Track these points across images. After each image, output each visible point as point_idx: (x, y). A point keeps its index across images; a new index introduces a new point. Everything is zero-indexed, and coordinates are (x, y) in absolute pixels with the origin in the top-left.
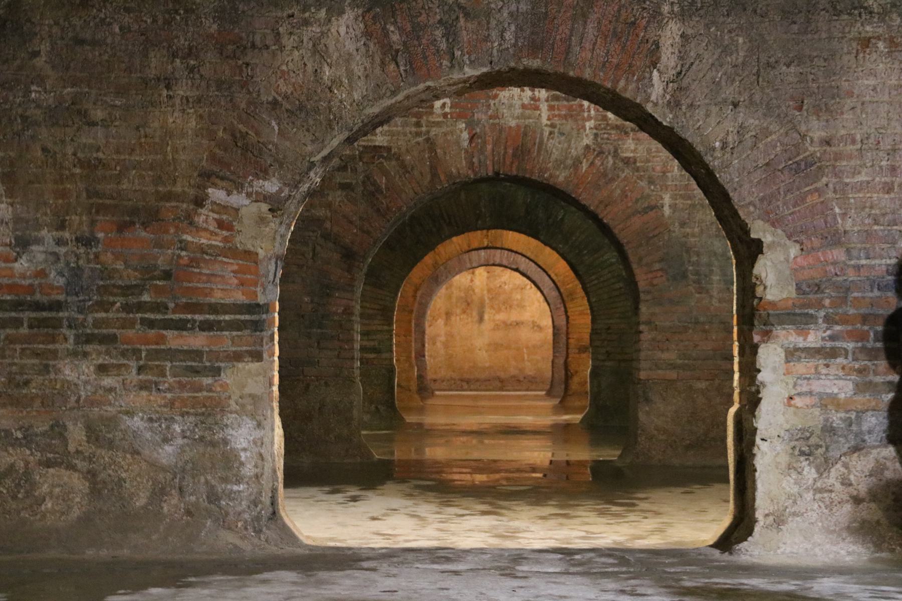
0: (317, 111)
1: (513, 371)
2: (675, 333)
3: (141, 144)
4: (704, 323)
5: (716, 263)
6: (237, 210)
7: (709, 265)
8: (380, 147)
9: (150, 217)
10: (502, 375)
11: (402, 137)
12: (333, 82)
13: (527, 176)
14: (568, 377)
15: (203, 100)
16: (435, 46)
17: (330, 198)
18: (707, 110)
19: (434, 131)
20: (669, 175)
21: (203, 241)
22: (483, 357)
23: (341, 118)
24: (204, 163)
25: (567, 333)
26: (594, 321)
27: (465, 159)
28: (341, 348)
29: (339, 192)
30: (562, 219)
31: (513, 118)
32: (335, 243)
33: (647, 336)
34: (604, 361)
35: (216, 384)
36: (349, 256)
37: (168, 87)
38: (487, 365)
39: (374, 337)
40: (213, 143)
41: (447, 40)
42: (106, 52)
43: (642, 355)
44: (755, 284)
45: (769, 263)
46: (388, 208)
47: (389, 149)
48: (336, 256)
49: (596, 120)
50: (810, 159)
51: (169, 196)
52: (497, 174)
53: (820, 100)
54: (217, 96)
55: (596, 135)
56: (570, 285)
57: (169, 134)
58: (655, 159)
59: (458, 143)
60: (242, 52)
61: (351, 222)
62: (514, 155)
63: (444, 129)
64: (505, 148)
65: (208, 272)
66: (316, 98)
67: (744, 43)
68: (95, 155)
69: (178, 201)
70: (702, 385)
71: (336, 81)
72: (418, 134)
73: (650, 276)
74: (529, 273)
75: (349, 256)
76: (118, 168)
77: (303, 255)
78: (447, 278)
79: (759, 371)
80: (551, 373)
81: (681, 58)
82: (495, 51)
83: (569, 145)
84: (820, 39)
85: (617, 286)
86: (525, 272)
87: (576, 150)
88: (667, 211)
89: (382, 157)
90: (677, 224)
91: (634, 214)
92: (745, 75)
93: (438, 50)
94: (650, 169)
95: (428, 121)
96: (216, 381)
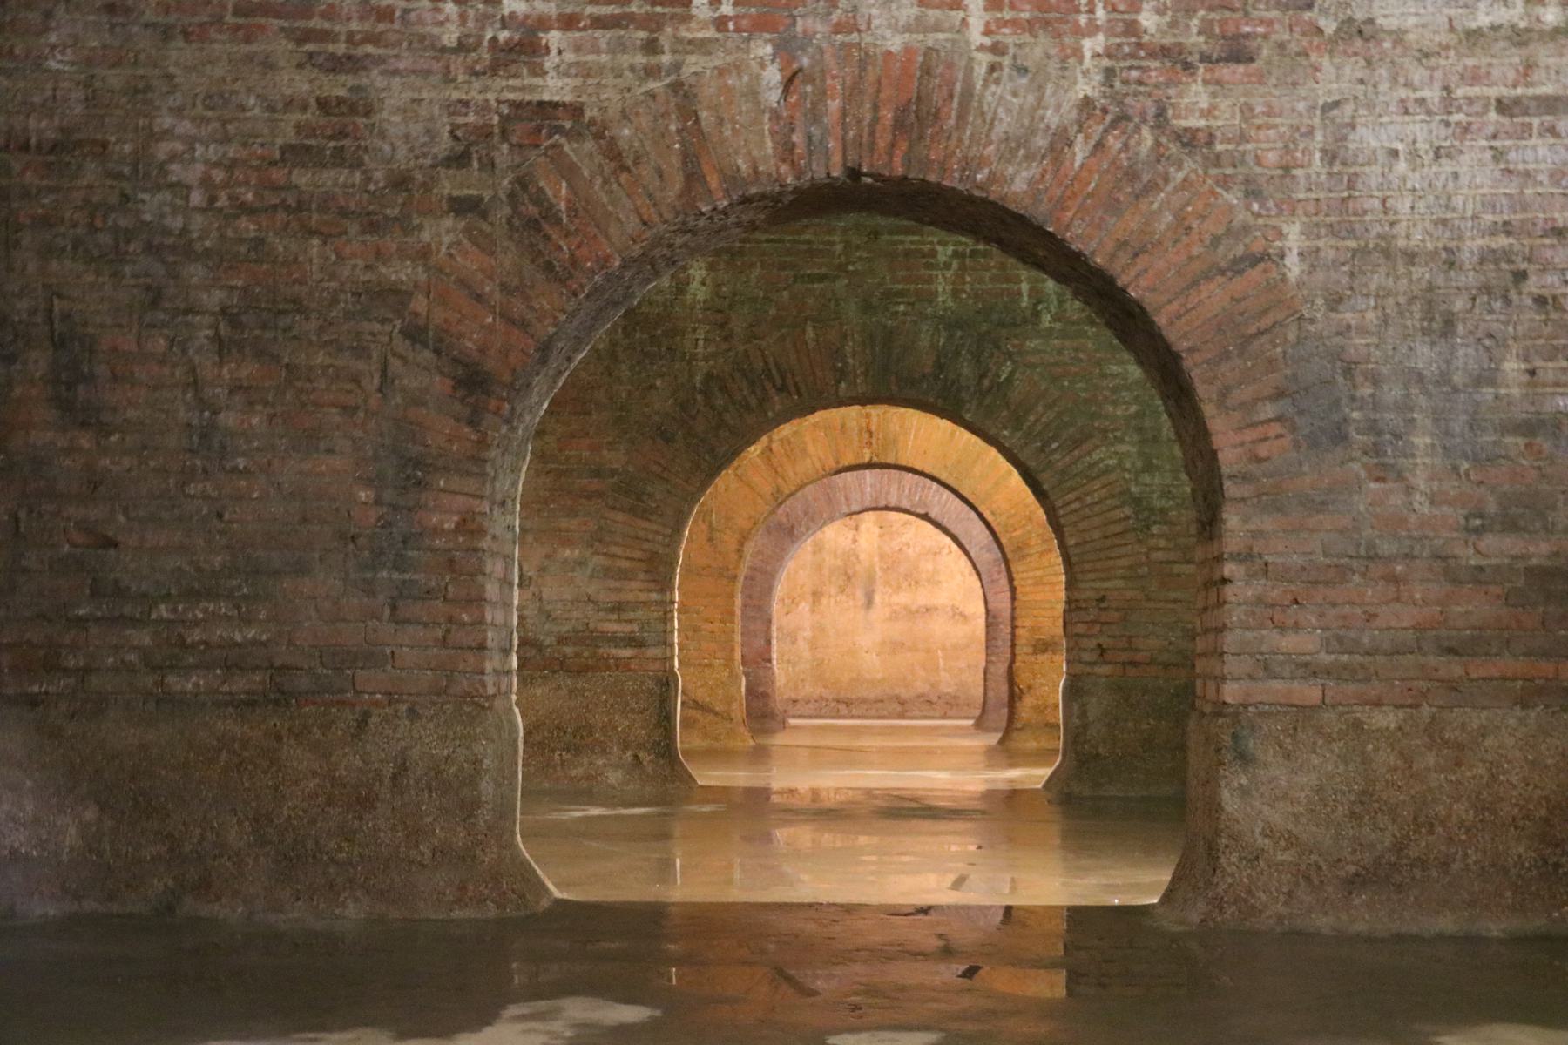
1: (921, 687)
2: (1316, 582)
4: (1391, 559)
5: (1422, 401)
7: (1405, 407)
8: (555, 105)
10: (904, 693)
11: (609, 80)
13: (932, 178)
14: (1014, 697)
17: (426, 236)
19: (694, 64)
20: (1298, 172)
22: (872, 664)
25: (1013, 618)
26: (1071, 585)
27: (773, 133)
28: (450, 620)
29: (448, 222)
30: (1009, 380)
31: (896, 29)
32: (437, 352)
33: (1241, 589)
34: (1094, 663)
36: (474, 384)
38: (879, 676)
39: (632, 615)
43: (1230, 640)
46: (574, 261)
47: (576, 110)
48: (440, 385)
49: (1110, 32)
52: (854, 173)
55: (1109, 73)
56: (1018, 533)
58: (1262, 134)
59: (753, 93)
61: (479, 298)
62: (899, 125)
63: (718, 60)
64: (876, 108)
70: (1386, 719)
72: (651, 72)
73: (1249, 435)
74: (945, 523)
75: (474, 384)
77: (356, 380)
78: (808, 529)
80: (981, 690)
83: (1040, 99)
85: (1118, 514)
86: (939, 519)
88: (1293, 267)
89: (559, 130)
90: (1320, 301)
91: (1207, 277)
94: (1250, 159)
95: (679, 40)
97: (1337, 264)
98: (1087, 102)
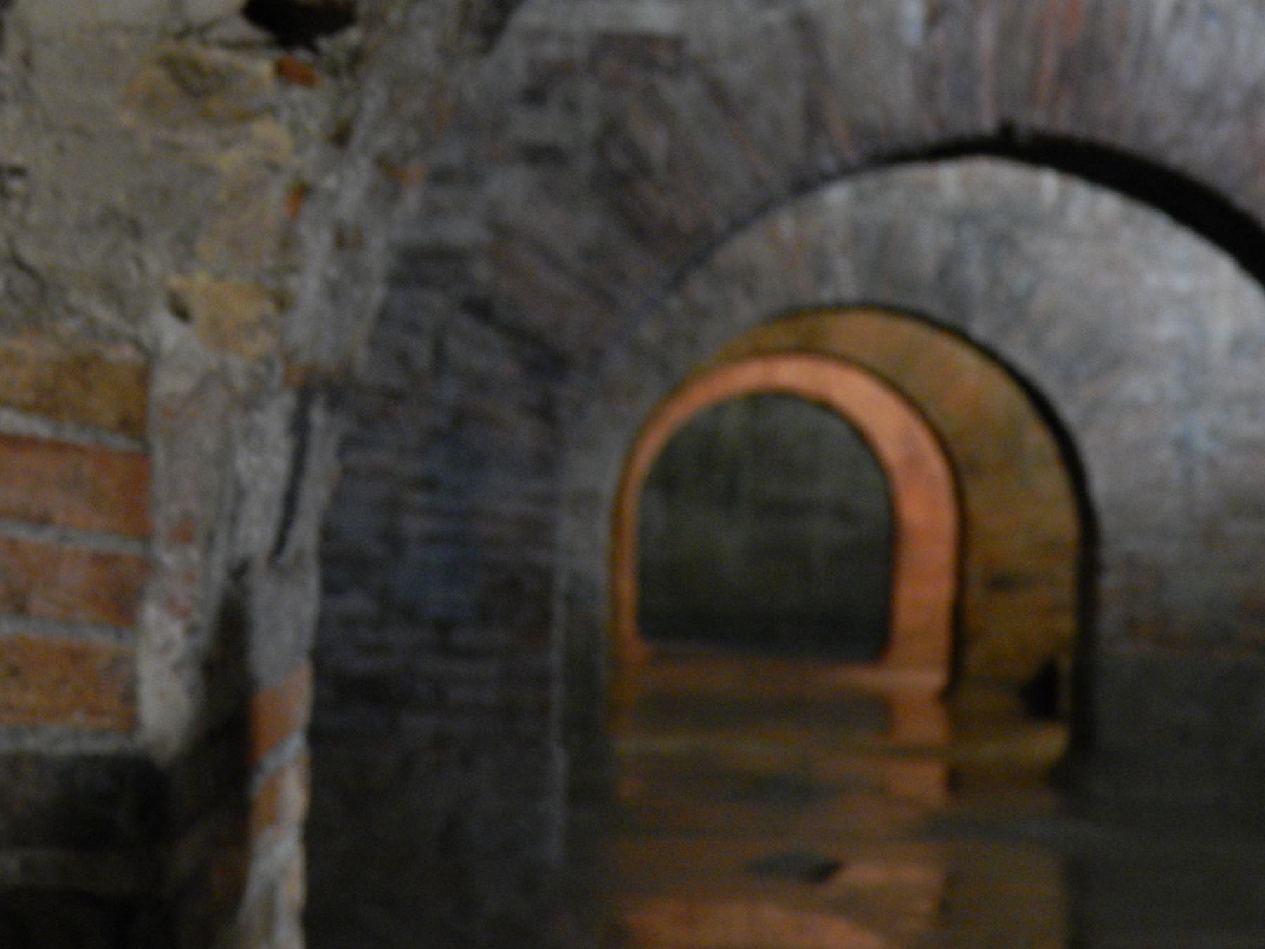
47: (676, 43)
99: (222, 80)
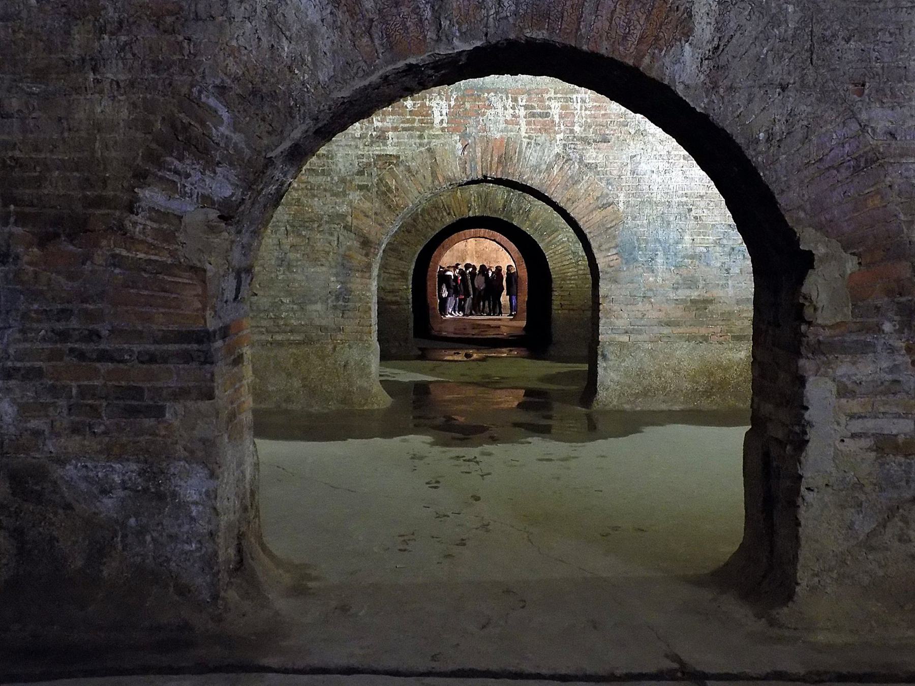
0: (274, 95)
3: (64, 139)
6: (180, 218)
9: (78, 228)
12: (294, 60)
13: (510, 178)
15: (136, 85)
16: (417, 14)
17: (351, 197)
18: (750, 94)
19: (435, 142)
21: (141, 255)
23: (304, 104)
24: (139, 161)
35: (160, 426)
36: (366, 243)
37: (95, 70)
40: (150, 137)
41: (433, 7)
42: (20, 28)
44: (804, 305)
45: (820, 281)
46: (397, 205)
47: (398, 157)
48: (357, 244)
50: (870, 154)
51: (99, 202)
53: (885, 83)
54: (153, 78)
57: (98, 127)
60: (183, 25)
62: (499, 162)
65: (146, 293)
66: (272, 80)
67: (795, 12)
68: (10, 154)
69: (109, 208)
71: (298, 61)
72: (421, 145)
73: (607, 259)
76: (38, 169)
77: (330, 243)
79: (807, 408)
81: (718, 30)
82: (491, 19)
84: (885, 10)
87: (549, 157)
88: (621, 206)
91: (595, 209)
92: (795, 51)
93: (421, 20)
95: (430, 135)
96: (159, 423)
97: (634, 206)
98: (558, 155)
99: (216, 227)
